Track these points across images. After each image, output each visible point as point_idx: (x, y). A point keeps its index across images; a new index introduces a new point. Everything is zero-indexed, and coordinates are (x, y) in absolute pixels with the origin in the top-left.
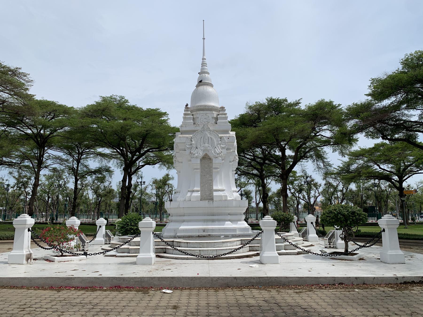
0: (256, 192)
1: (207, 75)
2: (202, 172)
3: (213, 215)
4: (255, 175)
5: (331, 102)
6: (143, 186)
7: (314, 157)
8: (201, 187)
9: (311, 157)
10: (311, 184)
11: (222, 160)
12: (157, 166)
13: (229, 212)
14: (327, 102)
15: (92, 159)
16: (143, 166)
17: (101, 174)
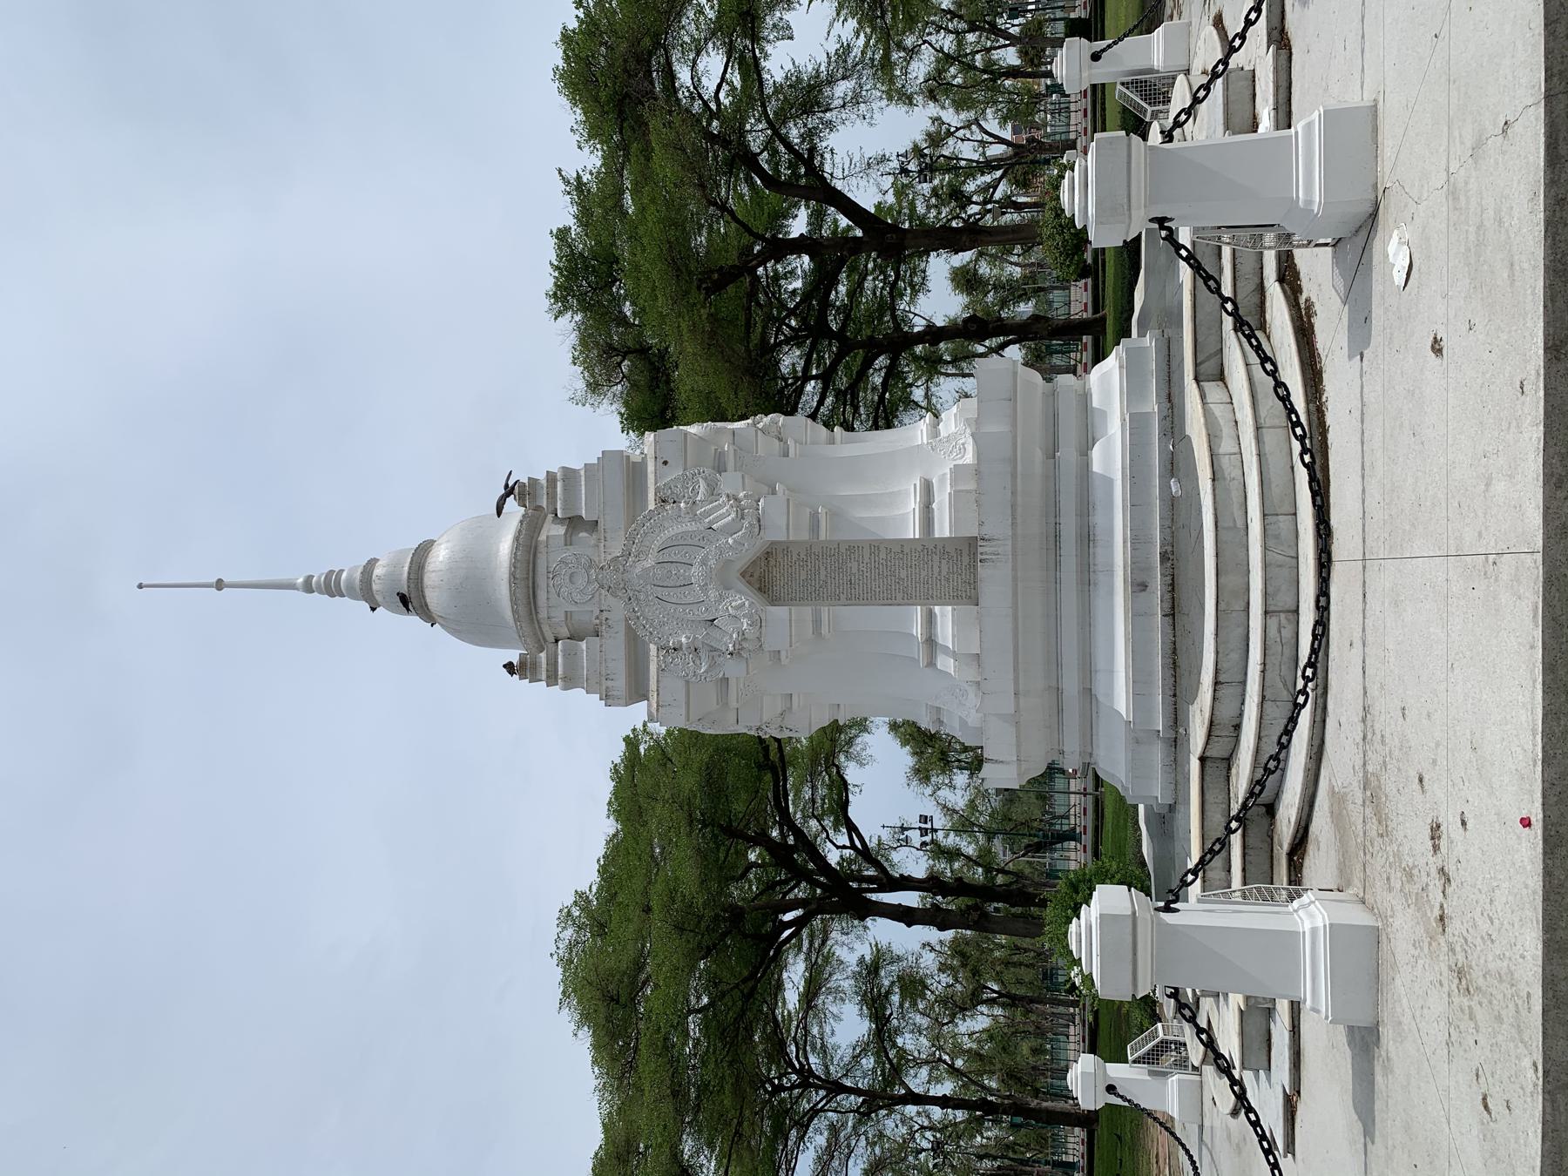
0: (964, 376)
1: (378, 571)
2: (835, 598)
3: (1057, 537)
4: (893, 373)
5: (567, 38)
6: (940, 821)
7: (812, 122)
8: (909, 600)
9: (810, 135)
10: (929, 159)
11: (774, 492)
12: (852, 773)
13: (1039, 455)
14: (567, 59)
15: (828, 1029)
16: (852, 828)
17: (888, 993)
